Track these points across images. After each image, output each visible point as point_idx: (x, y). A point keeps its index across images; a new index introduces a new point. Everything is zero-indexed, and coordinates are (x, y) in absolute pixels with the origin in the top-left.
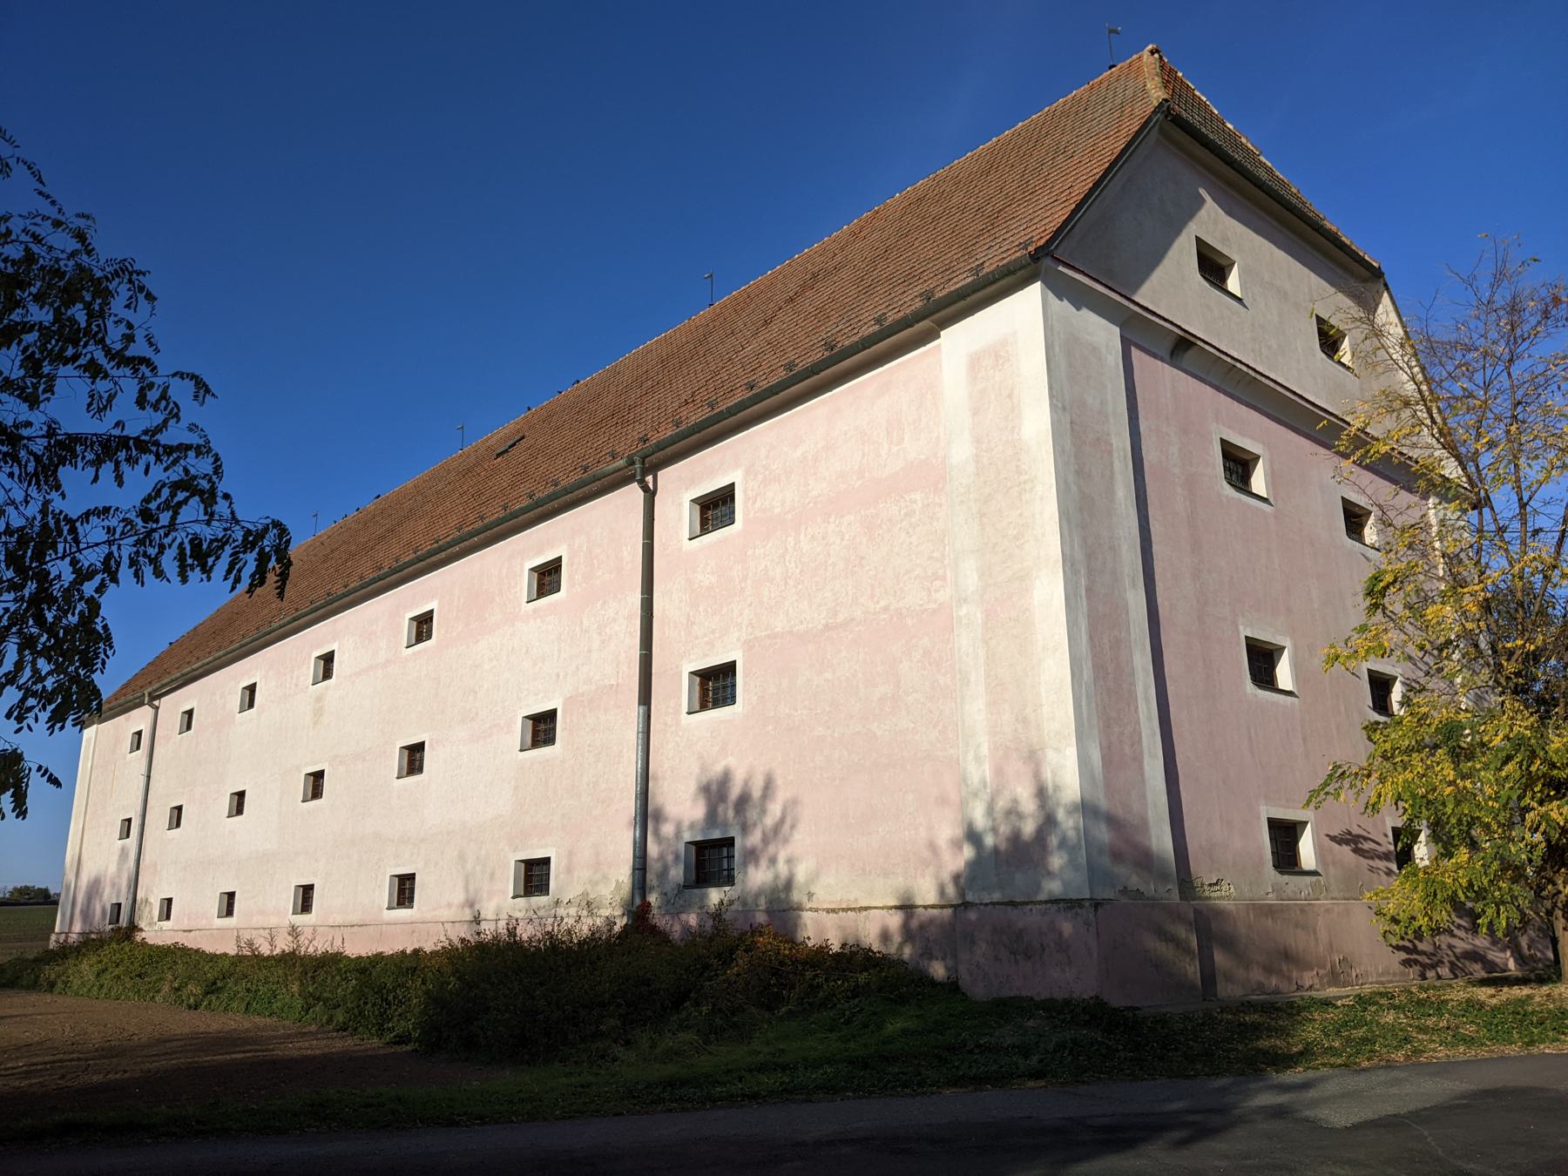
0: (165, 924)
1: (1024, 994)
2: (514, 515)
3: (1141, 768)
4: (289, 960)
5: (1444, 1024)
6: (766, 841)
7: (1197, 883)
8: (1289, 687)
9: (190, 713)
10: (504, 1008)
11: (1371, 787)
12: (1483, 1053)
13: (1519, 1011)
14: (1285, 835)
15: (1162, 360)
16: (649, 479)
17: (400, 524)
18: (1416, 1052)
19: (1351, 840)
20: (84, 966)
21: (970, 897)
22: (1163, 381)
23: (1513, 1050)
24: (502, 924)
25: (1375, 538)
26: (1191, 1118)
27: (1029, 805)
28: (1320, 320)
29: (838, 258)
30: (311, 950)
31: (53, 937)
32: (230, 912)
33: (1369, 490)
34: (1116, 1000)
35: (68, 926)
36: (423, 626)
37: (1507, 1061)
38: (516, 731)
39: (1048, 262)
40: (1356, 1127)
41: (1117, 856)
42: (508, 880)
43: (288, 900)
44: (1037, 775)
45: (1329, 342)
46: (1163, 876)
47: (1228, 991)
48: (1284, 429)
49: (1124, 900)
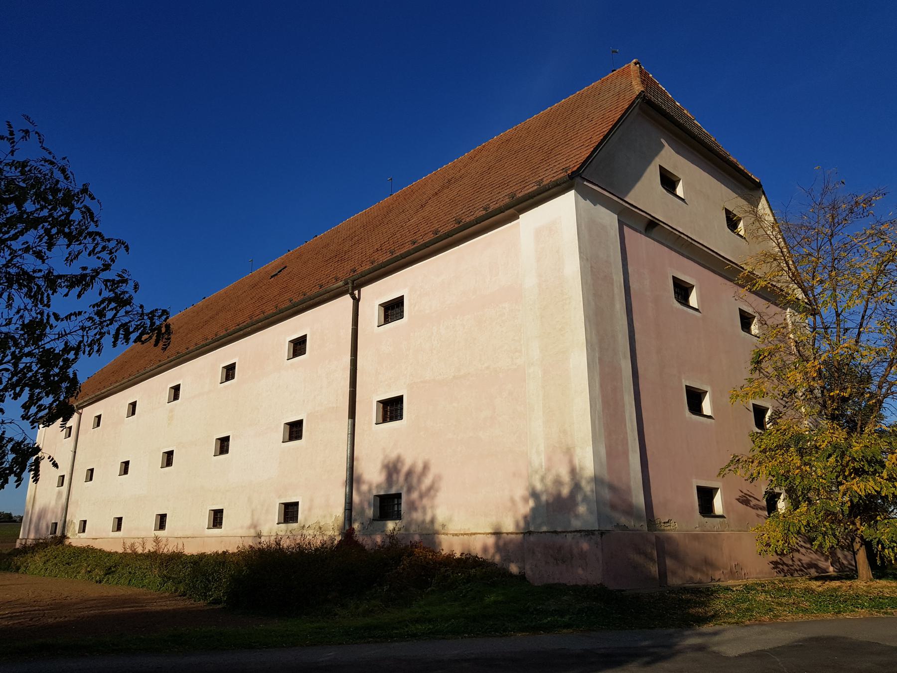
0: (82, 535)
1: (562, 581)
2: (281, 311)
4: (153, 556)
5: (791, 601)
6: (421, 497)
7: (658, 522)
8: (742, 233)
9: (99, 417)
10: (270, 585)
11: (753, 468)
12: (812, 618)
13: (833, 596)
14: (706, 495)
15: (640, 233)
16: (356, 292)
17: (217, 314)
18: (775, 616)
20: (37, 558)
21: (532, 529)
22: (639, 242)
23: (829, 616)
24: (272, 538)
25: (757, 331)
26: (651, 650)
27: (566, 477)
28: (728, 212)
29: (462, 172)
30: (165, 551)
31: (18, 541)
32: (119, 528)
34: (612, 586)
35: (26, 535)
36: (230, 372)
37: (825, 623)
38: (280, 432)
39: (578, 179)
40: (740, 656)
41: (613, 507)
42: (275, 514)
43: (152, 522)
44: (571, 462)
45: (732, 222)
46: (638, 517)
47: (674, 581)
48: (706, 271)
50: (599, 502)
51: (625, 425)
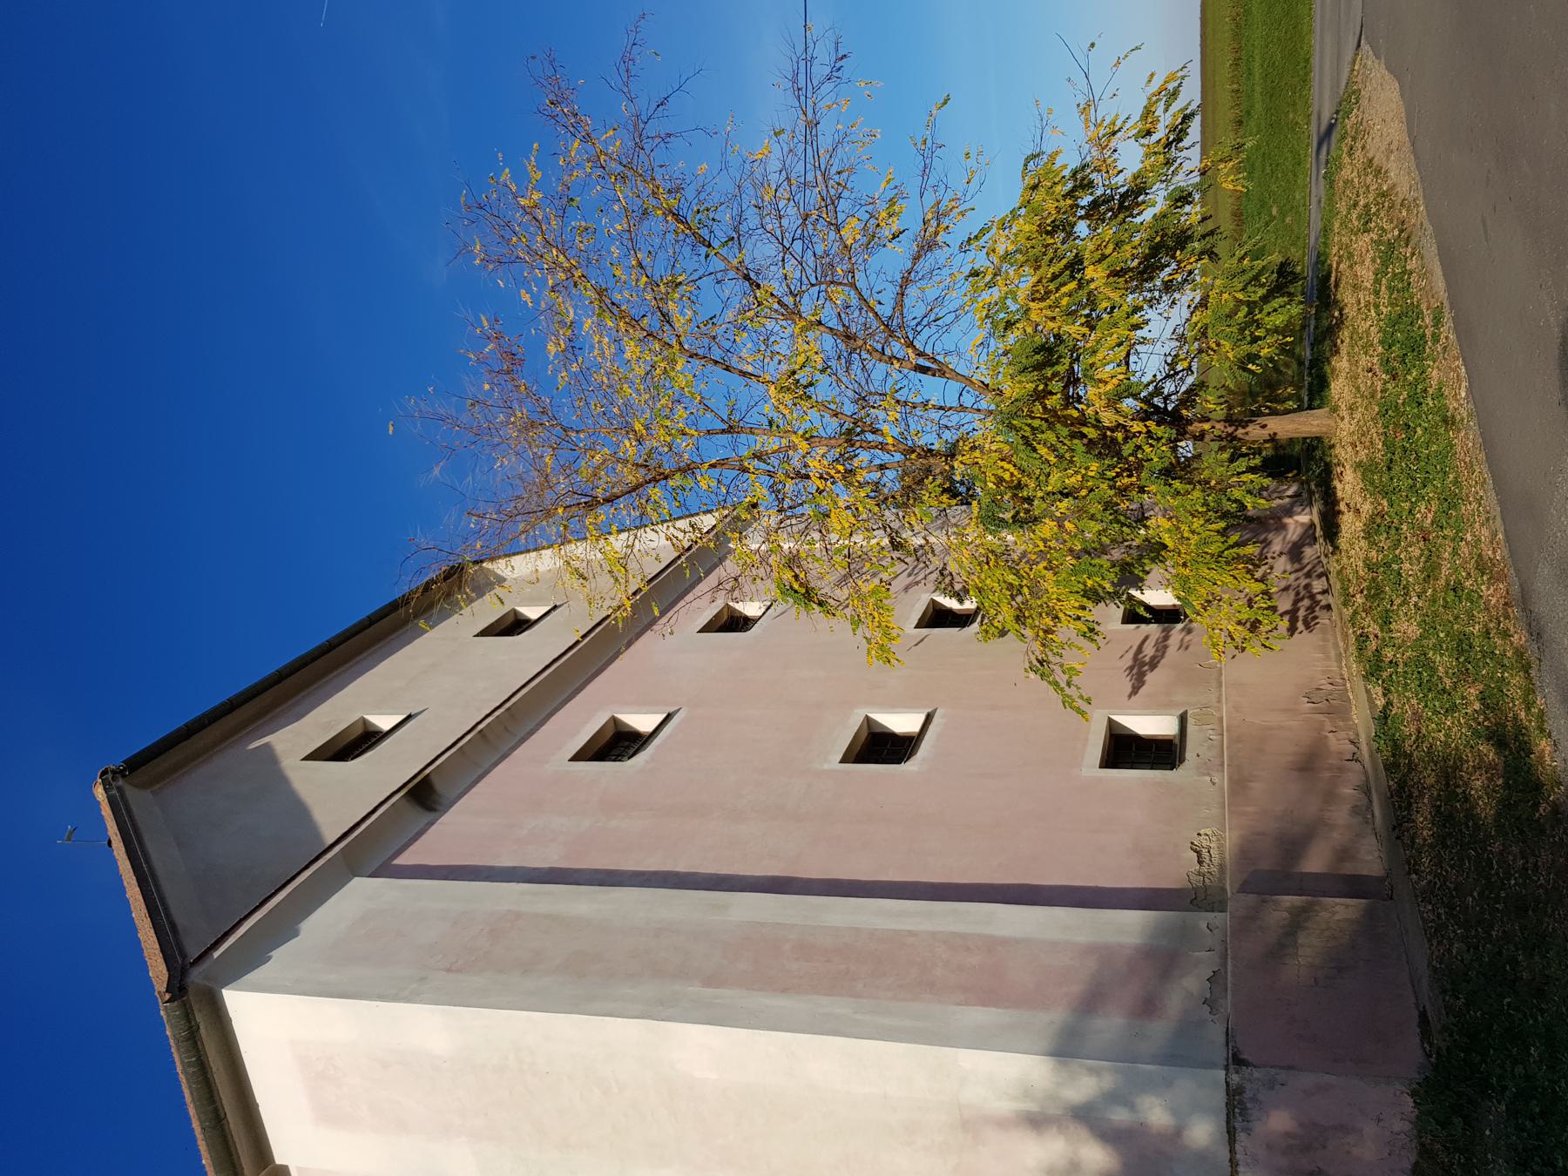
3: (1004, 941)
8: (920, 719)
14: (1125, 750)
19: (1140, 669)
22: (454, 832)
25: (757, 604)
33: (702, 606)
34: (1411, 1053)
39: (196, 976)
41: (1148, 1007)
44: (1002, 1124)
49: (1227, 1005)
50: (1124, 1055)
51: (911, 933)
